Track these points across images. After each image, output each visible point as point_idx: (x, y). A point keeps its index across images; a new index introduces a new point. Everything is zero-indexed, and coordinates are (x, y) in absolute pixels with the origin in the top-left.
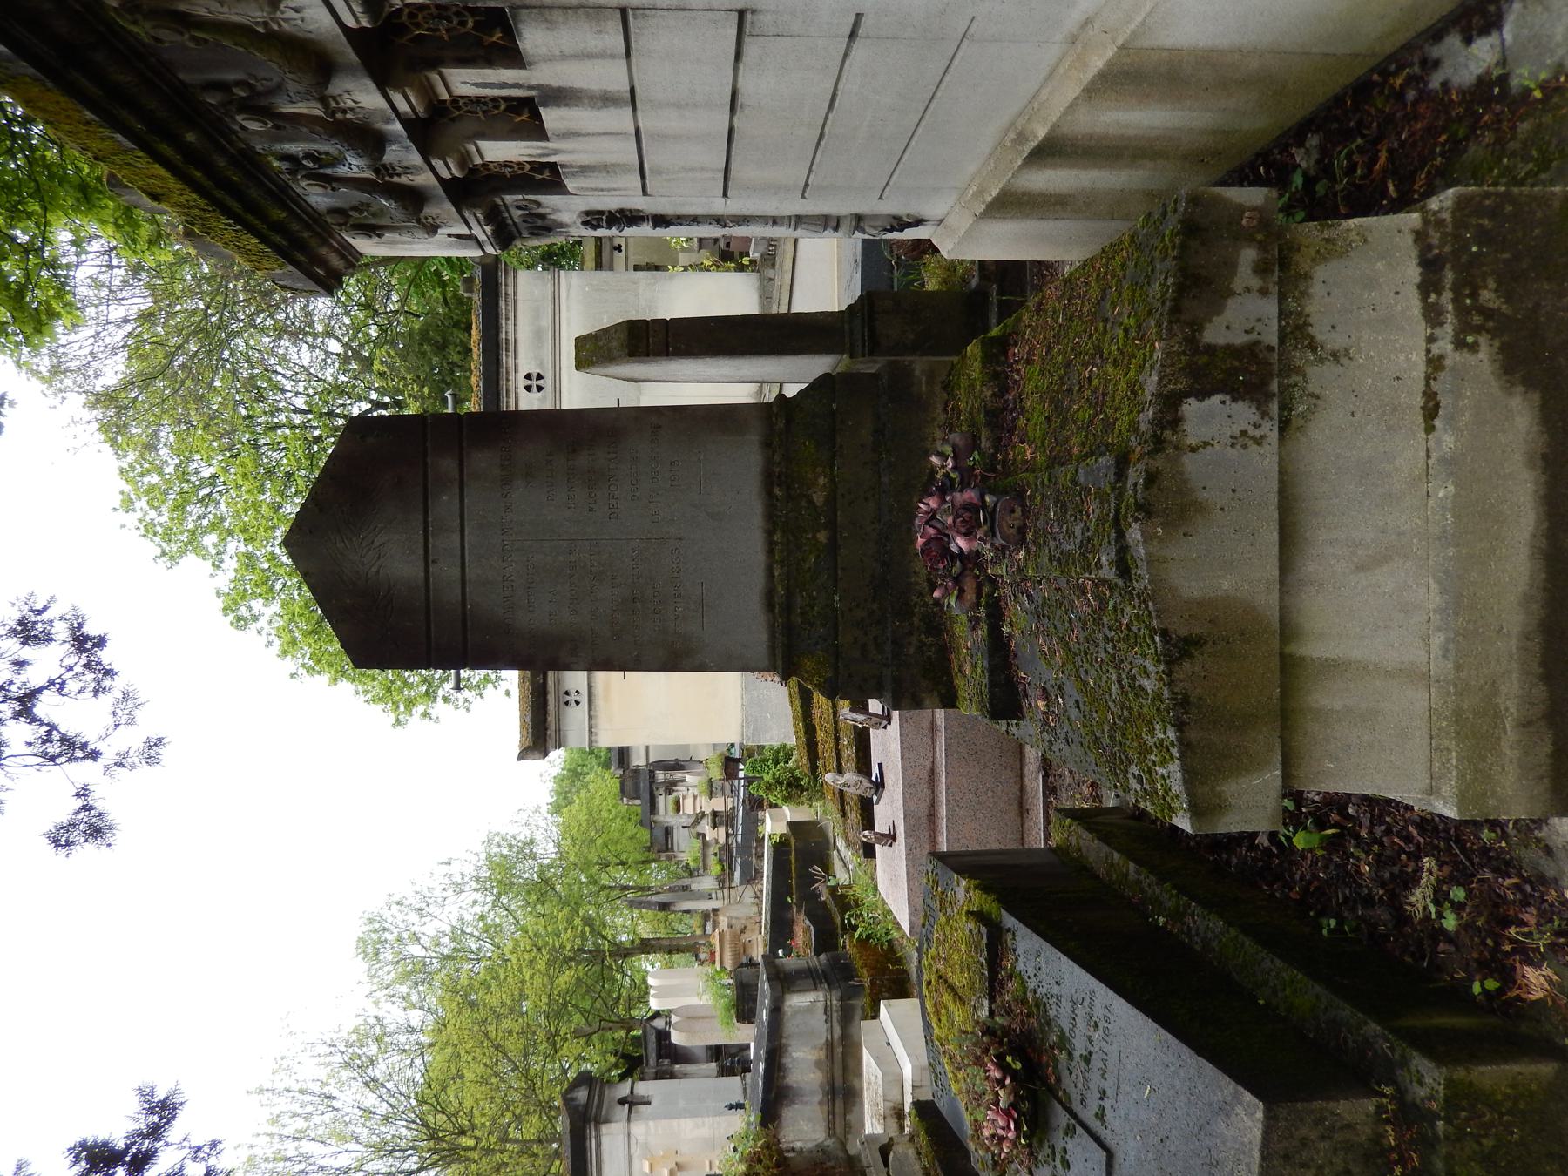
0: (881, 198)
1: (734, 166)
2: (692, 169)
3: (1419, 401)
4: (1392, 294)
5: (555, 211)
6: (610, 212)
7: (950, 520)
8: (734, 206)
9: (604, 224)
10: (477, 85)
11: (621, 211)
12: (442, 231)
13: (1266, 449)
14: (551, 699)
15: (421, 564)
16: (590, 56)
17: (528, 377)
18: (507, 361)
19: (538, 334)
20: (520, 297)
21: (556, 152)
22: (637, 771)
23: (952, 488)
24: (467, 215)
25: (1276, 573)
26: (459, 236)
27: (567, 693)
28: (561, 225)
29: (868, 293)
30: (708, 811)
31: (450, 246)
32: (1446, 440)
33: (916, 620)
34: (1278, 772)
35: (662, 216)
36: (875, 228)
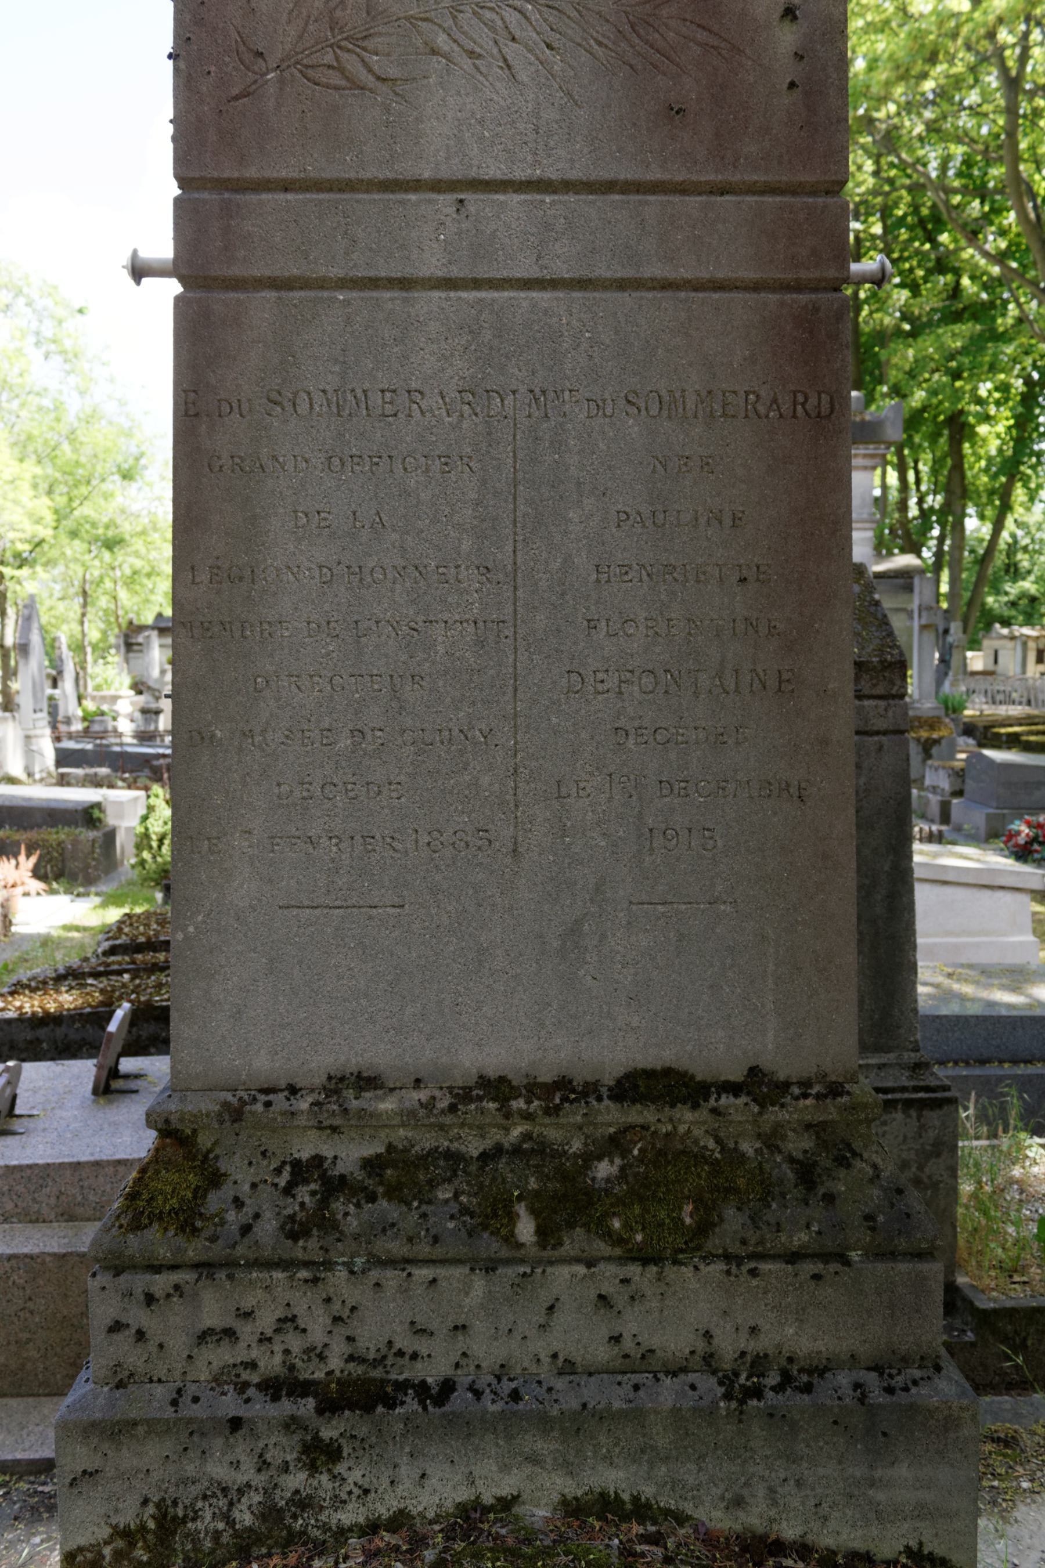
33: (296, 1480)
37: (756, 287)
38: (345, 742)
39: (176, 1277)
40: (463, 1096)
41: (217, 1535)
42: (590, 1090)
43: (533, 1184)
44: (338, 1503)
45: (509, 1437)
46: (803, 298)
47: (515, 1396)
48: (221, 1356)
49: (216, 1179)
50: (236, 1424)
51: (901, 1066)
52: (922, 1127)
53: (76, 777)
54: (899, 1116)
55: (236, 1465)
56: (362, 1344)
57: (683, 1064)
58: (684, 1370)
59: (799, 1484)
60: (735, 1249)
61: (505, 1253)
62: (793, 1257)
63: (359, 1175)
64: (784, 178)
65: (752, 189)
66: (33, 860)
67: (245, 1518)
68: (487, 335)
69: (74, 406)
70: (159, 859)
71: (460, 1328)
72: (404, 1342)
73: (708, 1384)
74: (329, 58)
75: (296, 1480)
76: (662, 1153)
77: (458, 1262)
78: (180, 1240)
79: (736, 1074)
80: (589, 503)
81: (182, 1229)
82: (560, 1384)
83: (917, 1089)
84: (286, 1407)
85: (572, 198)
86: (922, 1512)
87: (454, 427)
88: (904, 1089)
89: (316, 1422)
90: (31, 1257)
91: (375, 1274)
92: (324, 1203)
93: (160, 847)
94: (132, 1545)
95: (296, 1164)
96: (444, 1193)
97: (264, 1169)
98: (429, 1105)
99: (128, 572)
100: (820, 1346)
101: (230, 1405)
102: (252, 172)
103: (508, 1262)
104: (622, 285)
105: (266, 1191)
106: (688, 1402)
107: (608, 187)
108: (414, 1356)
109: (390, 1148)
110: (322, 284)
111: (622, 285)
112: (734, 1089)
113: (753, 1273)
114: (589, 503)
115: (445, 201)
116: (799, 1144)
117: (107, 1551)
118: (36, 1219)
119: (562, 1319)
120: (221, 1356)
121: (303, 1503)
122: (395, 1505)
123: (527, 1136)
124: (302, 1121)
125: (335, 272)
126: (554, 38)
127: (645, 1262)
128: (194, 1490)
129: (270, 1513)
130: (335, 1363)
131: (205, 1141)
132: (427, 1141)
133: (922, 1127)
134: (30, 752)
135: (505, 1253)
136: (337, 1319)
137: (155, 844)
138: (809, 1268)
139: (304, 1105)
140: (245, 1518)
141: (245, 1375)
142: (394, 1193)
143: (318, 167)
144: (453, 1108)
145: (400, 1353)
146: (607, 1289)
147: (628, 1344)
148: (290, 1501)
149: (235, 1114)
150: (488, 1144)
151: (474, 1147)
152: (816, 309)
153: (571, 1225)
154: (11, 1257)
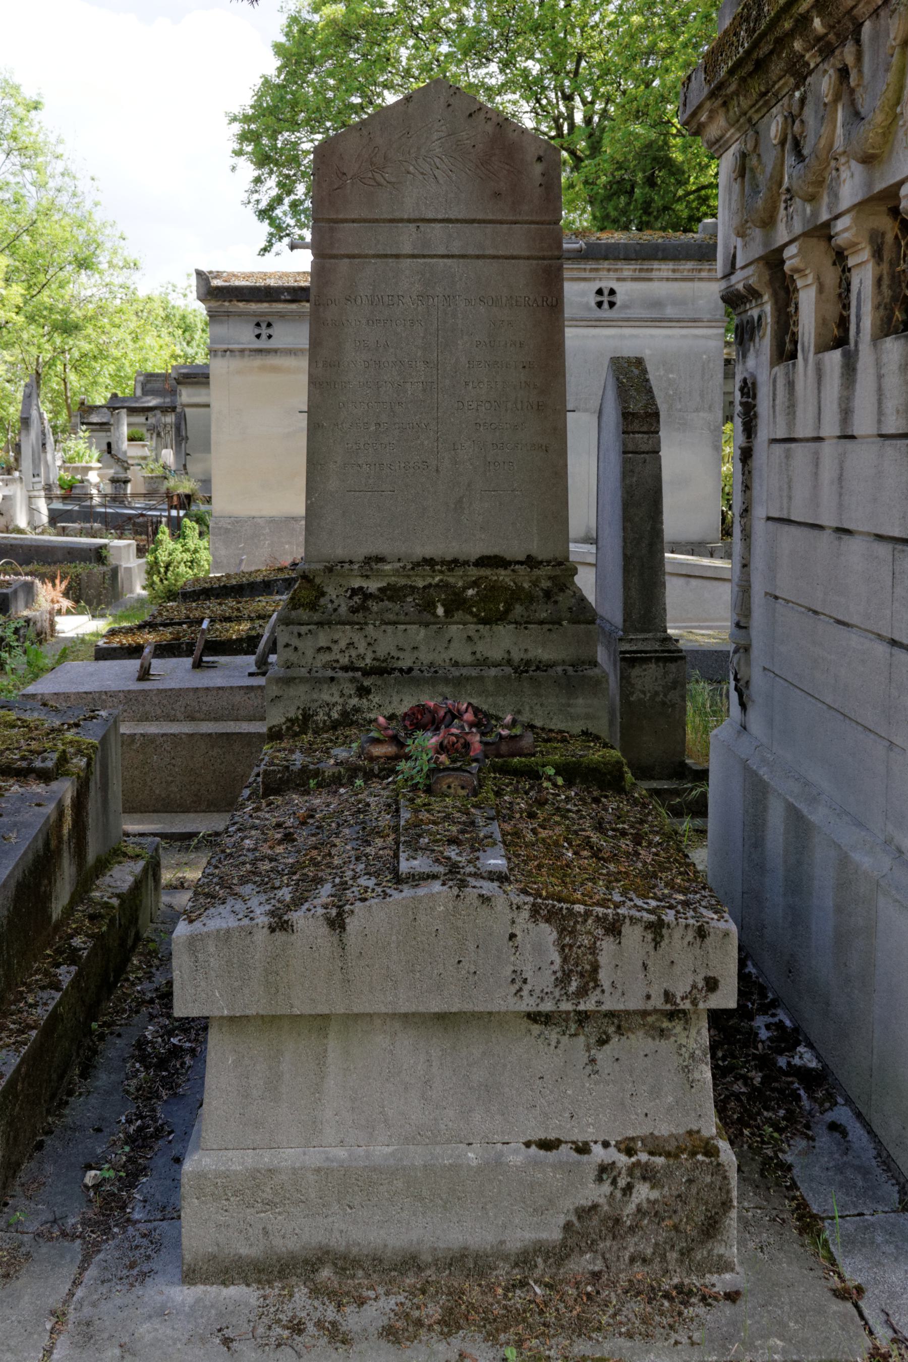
0: (765, 669)
1: (793, 529)
2: (790, 488)
3: (552, 1136)
4: (645, 1111)
5: (757, 353)
6: (755, 406)
7: (455, 731)
8: (759, 527)
9: (745, 400)
10: (859, 293)
11: (756, 416)
12: (739, 242)
13: (512, 1000)
14: (264, 307)
15: (415, 215)
16: (880, 402)
17: (612, 292)
18: (628, 269)
19: (657, 304)
20: (697, 285)
21: (806, 360)
22: (173, 393)
23: (483, 734)
24: (752, 268)
25: (403, 1010)
26: (734, 256)
27: (269, 325)
28: (744, 356)
29: (683, 658)
30: (130, 475)
31: (726, 246)
32: (517, 1156)
33: (355, 701)
34: (226, 1013)
35: (751, 456)
36: (738, 663)
37: (528, 258)
38: (373, 428)
39: (309, 627)
40: (416, 565)
41: (325, 721)
42: (466, 563)
43: (443, 596)
44: (370, 710)
45: (433, 686)
46: (546, 262)
47: (436, 672)
48: (325, 657)
49: (323, 594)
50: (332, 679)
51: (656, 640)
52: (666, 673)
53: (75, 529)
54: (653, 666)
55: (332, 695)
56: (378, 654)
57: (502, 554)
58: (499, 665)
59: (542, 705)
60: (519, 619)
61: (432, 620)
62: (541, 623)
63: (377, 593)
64: (538, 219)
65: (526, 222)
66: (63, 586)
67: (335, 715)
68: (428, 275)
69: (32, 198)
70: (166, 582)
71: (415, 648)
72: (394, 653)
73: (509, 670)
74: (370, 175)
75: (355, 701)
76: (493, 587)
77: (414, 623)
78: (311, 613)
79: (522, 558)
80: (466, 338)
81: (311, 609)
82: (453, 669)
83: (663, 651)
84: (350, 674)
85: (459, 225)
86: (588, 717)
87: (416, 309)
88: (656, 651)
89: (362, 679)
90: (174, 735)
91: (383, 627)
92: (364, 601)
93: (166, 573)
94: (293, 724)
95: (353, 589)
96: (409, 599)
97: (341, 591)
98: (404, 568)
99: (76, 354)
100: (551, 657)
101: (330, 673)
102: (341, 216)
103: (434, 623)
104: (478, 257)
105: (342, 599)
106: (501, 674)
107: (472, 221)
108: (398, 659)
109: (389, 584)
110: (366, 256)
111: (478, 257)
112: (521, 563)
113: (526, 628)
114: (466, 338)
115: (412, 226)
116: (546, 584)
117: (284, 727)
118: (174, 720)
119: (454, 645)
120: (325, 657)
121: (357, 710)
122: (391, 711)
123: (441, 581)
124: (355, 573)
125: (371, 252)
126: (453, 168)
127: (485, 624)
128: (317, 704)
129: (344, 714)
130: (368, 661)
131: (318, 581)
132: (403, 582)
133: (666, 673)
134: (32, 511)
135: (432, 620)
136: (369, 644)
137: (162, 570)
138: (547, 626)
139: (356, 567)
140: (335, 715)
141: (335, 665)
142: (390, 599)
143: (365, 214)
144: (413, 569)
145: (393, 657)
146: (471, 634)
147: (478, 656)
148: (352, 709)
149: (330, 570)
150: (426, 583)
151: (420, 584)
152: (550, 266)
153: (457, 610)
154: (163, 735)
